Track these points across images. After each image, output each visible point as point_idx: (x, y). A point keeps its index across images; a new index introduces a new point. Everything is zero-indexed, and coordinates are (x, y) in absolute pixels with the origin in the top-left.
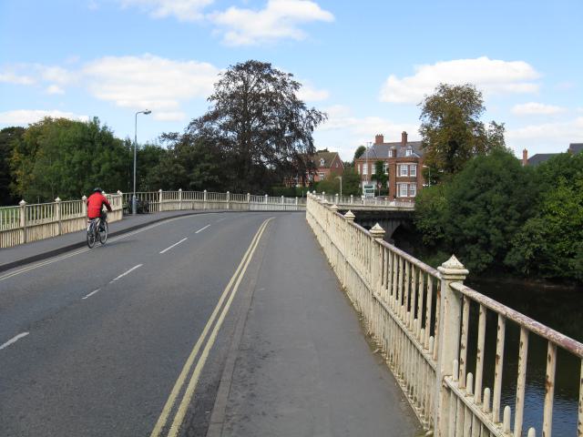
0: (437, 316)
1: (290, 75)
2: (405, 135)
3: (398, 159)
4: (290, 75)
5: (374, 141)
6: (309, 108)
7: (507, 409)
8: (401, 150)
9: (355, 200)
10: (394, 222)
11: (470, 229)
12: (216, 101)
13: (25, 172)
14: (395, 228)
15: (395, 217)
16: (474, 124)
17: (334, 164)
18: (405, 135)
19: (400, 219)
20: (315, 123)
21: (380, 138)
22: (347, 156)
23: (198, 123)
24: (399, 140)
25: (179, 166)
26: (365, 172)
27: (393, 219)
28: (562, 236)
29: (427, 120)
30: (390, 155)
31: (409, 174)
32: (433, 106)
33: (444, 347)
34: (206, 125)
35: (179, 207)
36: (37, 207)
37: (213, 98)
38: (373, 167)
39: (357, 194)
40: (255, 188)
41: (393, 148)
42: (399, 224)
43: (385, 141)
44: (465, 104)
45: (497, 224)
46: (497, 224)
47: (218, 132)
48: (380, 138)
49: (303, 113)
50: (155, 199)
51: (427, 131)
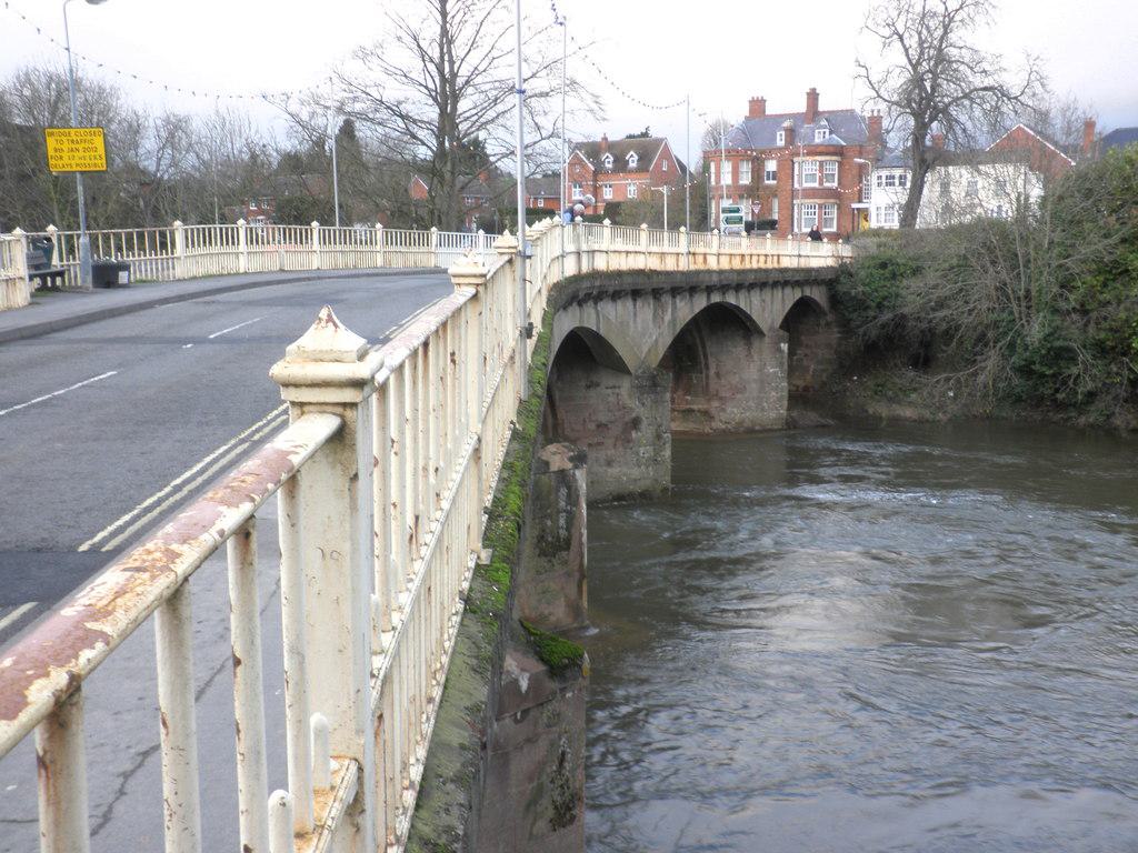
2: (813, 96)
4: (399, 39)
5: (745, 111)
8: (805, 129)
10: (788, 290)
14: (789, 305)
17: (659, 165)
18: (813, 96)
21: (757, 106)
22: (690, 154)
24: (801, 106)
26: (727, 180)
27: (785, 284)
28: (1073, 246)
30: (780, 142)
31: (821, 183)
33: (961, 679)
35: (316, 262)
36: (696, 235)
39: (702, 223)
41: (787, 124)
43: (769, 111)
44: (934, 397)
48: (757, 106)
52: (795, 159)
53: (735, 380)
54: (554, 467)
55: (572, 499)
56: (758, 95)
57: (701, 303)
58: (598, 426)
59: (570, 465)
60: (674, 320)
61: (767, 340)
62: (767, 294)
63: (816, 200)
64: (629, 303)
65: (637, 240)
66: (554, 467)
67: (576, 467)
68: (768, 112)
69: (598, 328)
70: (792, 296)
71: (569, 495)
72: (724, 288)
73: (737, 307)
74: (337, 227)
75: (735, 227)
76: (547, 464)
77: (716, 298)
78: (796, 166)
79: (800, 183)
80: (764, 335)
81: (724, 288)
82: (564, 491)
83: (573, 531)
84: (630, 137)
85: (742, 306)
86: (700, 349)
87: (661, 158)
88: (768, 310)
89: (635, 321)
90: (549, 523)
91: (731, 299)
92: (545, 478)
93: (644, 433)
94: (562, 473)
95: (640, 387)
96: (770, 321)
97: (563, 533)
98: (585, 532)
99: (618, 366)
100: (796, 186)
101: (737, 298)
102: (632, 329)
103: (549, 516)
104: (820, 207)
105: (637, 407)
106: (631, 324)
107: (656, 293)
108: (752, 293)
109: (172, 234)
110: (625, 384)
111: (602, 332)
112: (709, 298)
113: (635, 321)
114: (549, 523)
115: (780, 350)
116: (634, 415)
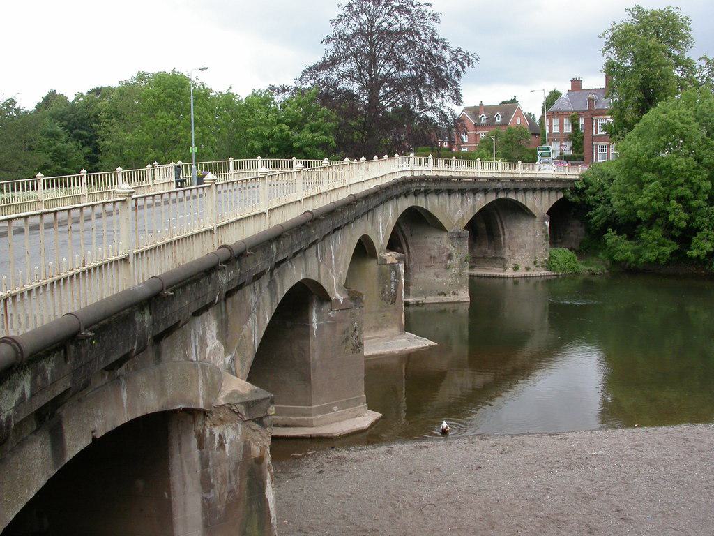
0: (437, 301)
1: (428, 5)
2: (515, 97)
3: (593, 114)
4: (428, 5)
6: (454, 46)
7: (210, 381)
9: (91, 182)
10: (553, 194)
11: (645, 209)
12: (332, 45)
13: (116, 136)
15: (545, 186)
16: (678, 62)
18: (515, 97)
19: (563, 190)
20: (463, 67)
23: (311, 71)
25: (284, 126)
26: (556, 130)
29: (613, 55)
32: (621, 39)
34: (323, 75)
37: (329, 40)
38: (566, 122)
40: (299, 155)
42: (561, 196)
45: (680, 199)
46: (680, 199)
47: (336, 84)
49: (447, 55)
50: (225, 169)
51: (611, 70)
52: (594, 118)
53: (520, 241)
54: (389, 262)
55: (397, 275)
56: (576, 76)
57: (491, 198)
58: (431, 257)
59: (396, 261)
60: (474, 207)
61: (537, 219)
62: (538, 195)
63: (606, 143)
64: (447, 197)
65: (291, 166)
66: (389, 262)
67: (399, 262)
68: (583, 88)
69: (427, 207)
70: (555, 198)
71: (396, 274)
72: (507, 191)
73: (517, 201)
74: (194, 163)
75: (546, 159)
76: (386, 260)
77: (501, 196)
78: (594, 121)
79: (597, 133)
80: (536, 217)
81: (507, 191)
82: (393, 273)
83: (398, 291)
84: (504, 103)
85: (520, 200)
86: (499, 224)
87: (516, 116)
88: (540, 204)
89: (450, 205)
90: (387, 286)
91: (512, 196)
92: (384, 266)
93: (455, 261)
94: (392, 264)
95: (452, 238)
96: (540, 210)
97: (393, 291)
98: (403, 291)
99: (440, 227)
100: (594, 133)
101: (517, 196)
102: (448, 209)
103: (386, 283)
104: (609, 146)
105: (452, 249)
106: (448, 206)
107: (462, 192)
108: (527, 194)
109: (229, 163)
110: (445, 236)
111: (429, 209)
112: (496, 196)
113: (450, 205)
114: (387, 286)
115: (544, 225)
116: (449, 252)
